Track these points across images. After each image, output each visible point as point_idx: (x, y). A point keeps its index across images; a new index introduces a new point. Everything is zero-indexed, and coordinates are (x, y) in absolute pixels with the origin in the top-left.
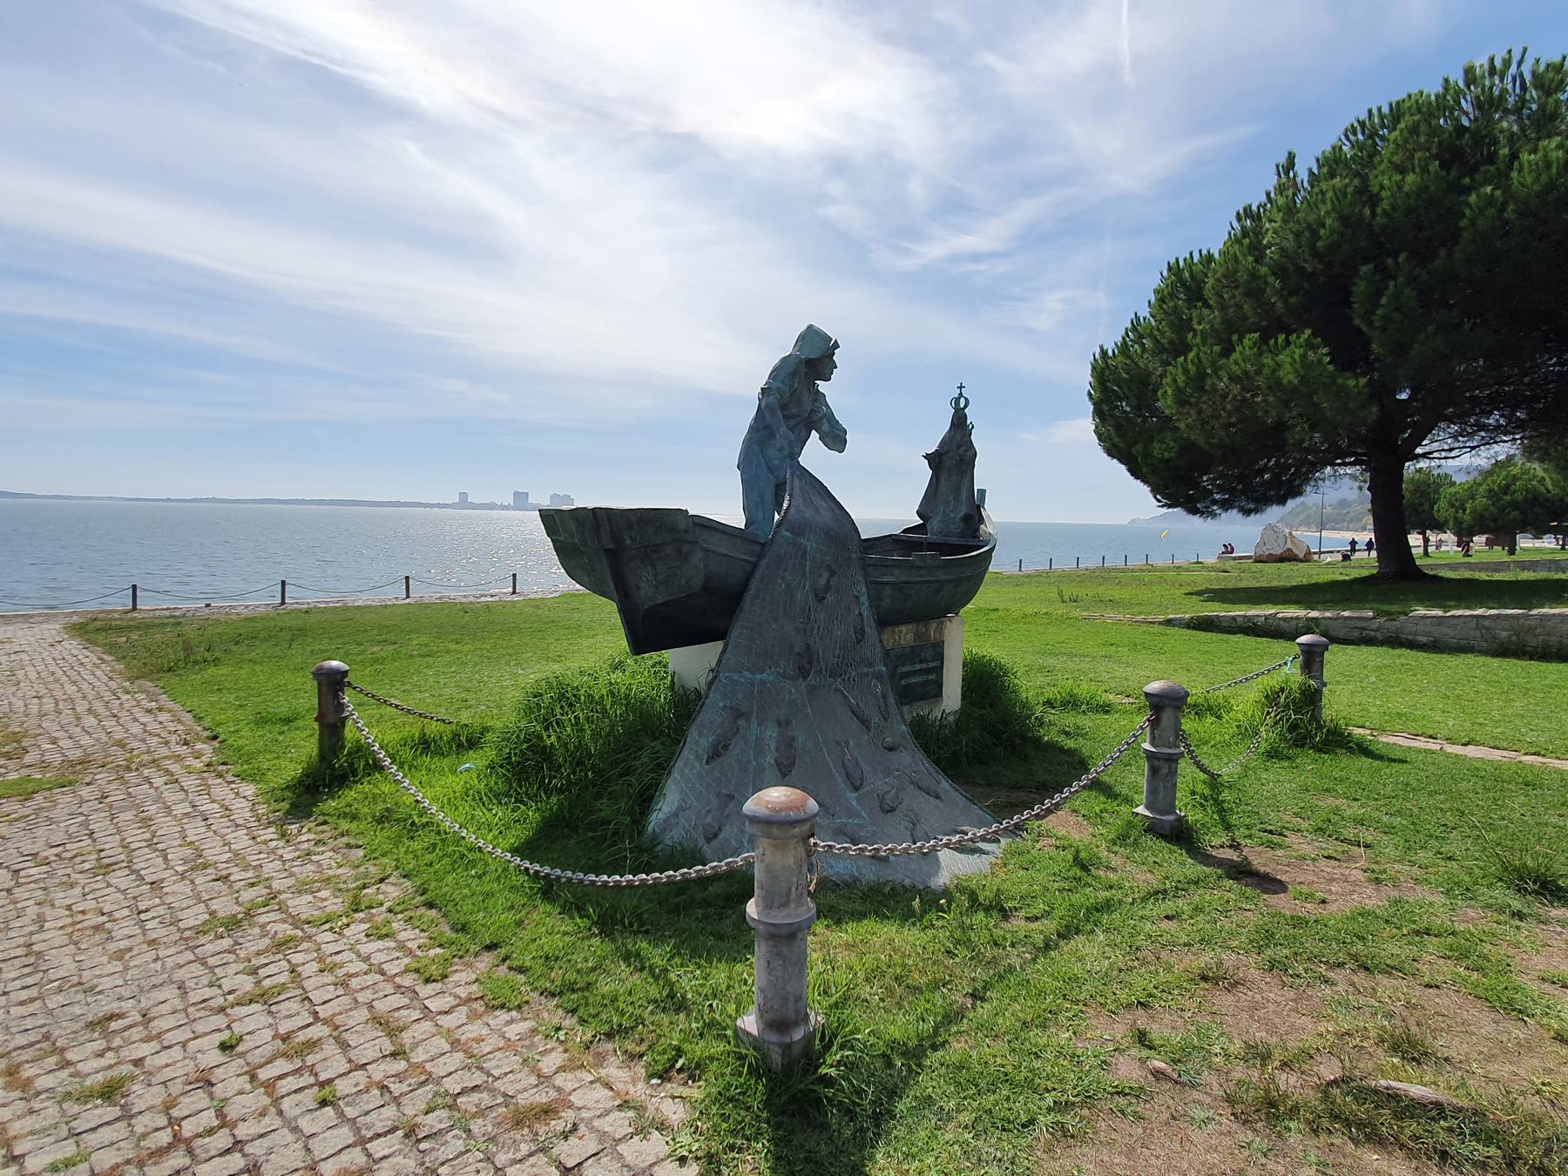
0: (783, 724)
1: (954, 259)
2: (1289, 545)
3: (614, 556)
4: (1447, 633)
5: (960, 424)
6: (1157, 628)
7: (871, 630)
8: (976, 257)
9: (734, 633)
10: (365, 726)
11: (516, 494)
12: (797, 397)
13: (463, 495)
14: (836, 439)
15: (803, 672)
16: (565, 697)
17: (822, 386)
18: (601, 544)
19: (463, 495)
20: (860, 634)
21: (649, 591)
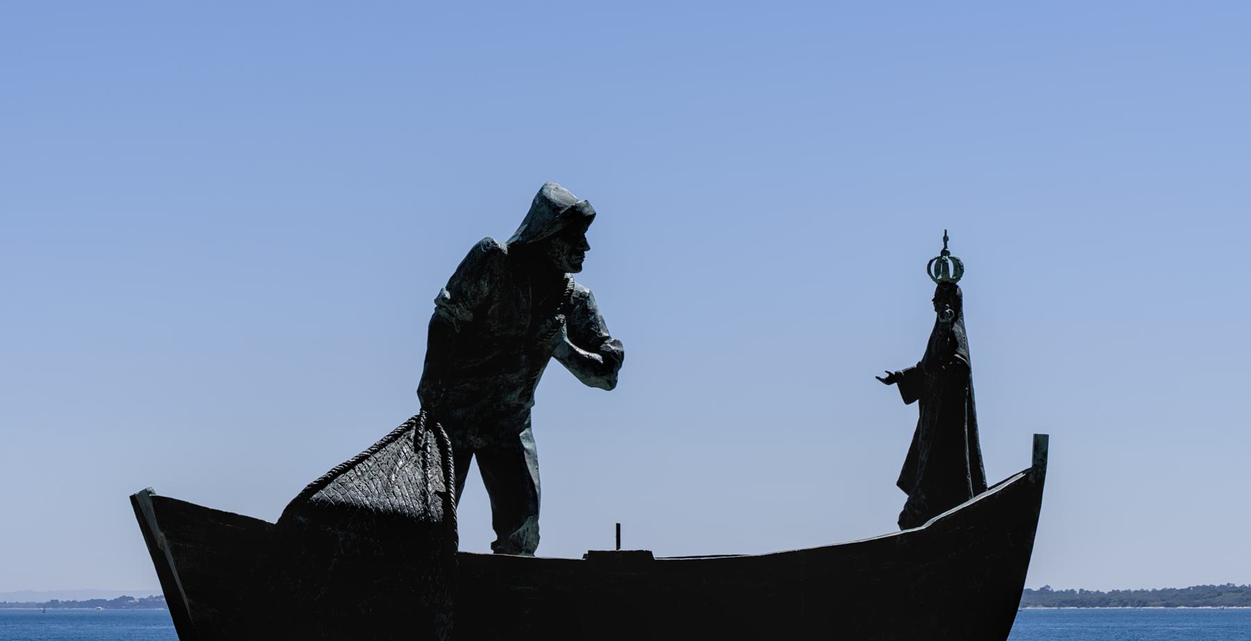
5: (948, 298)
17: (577, 282)
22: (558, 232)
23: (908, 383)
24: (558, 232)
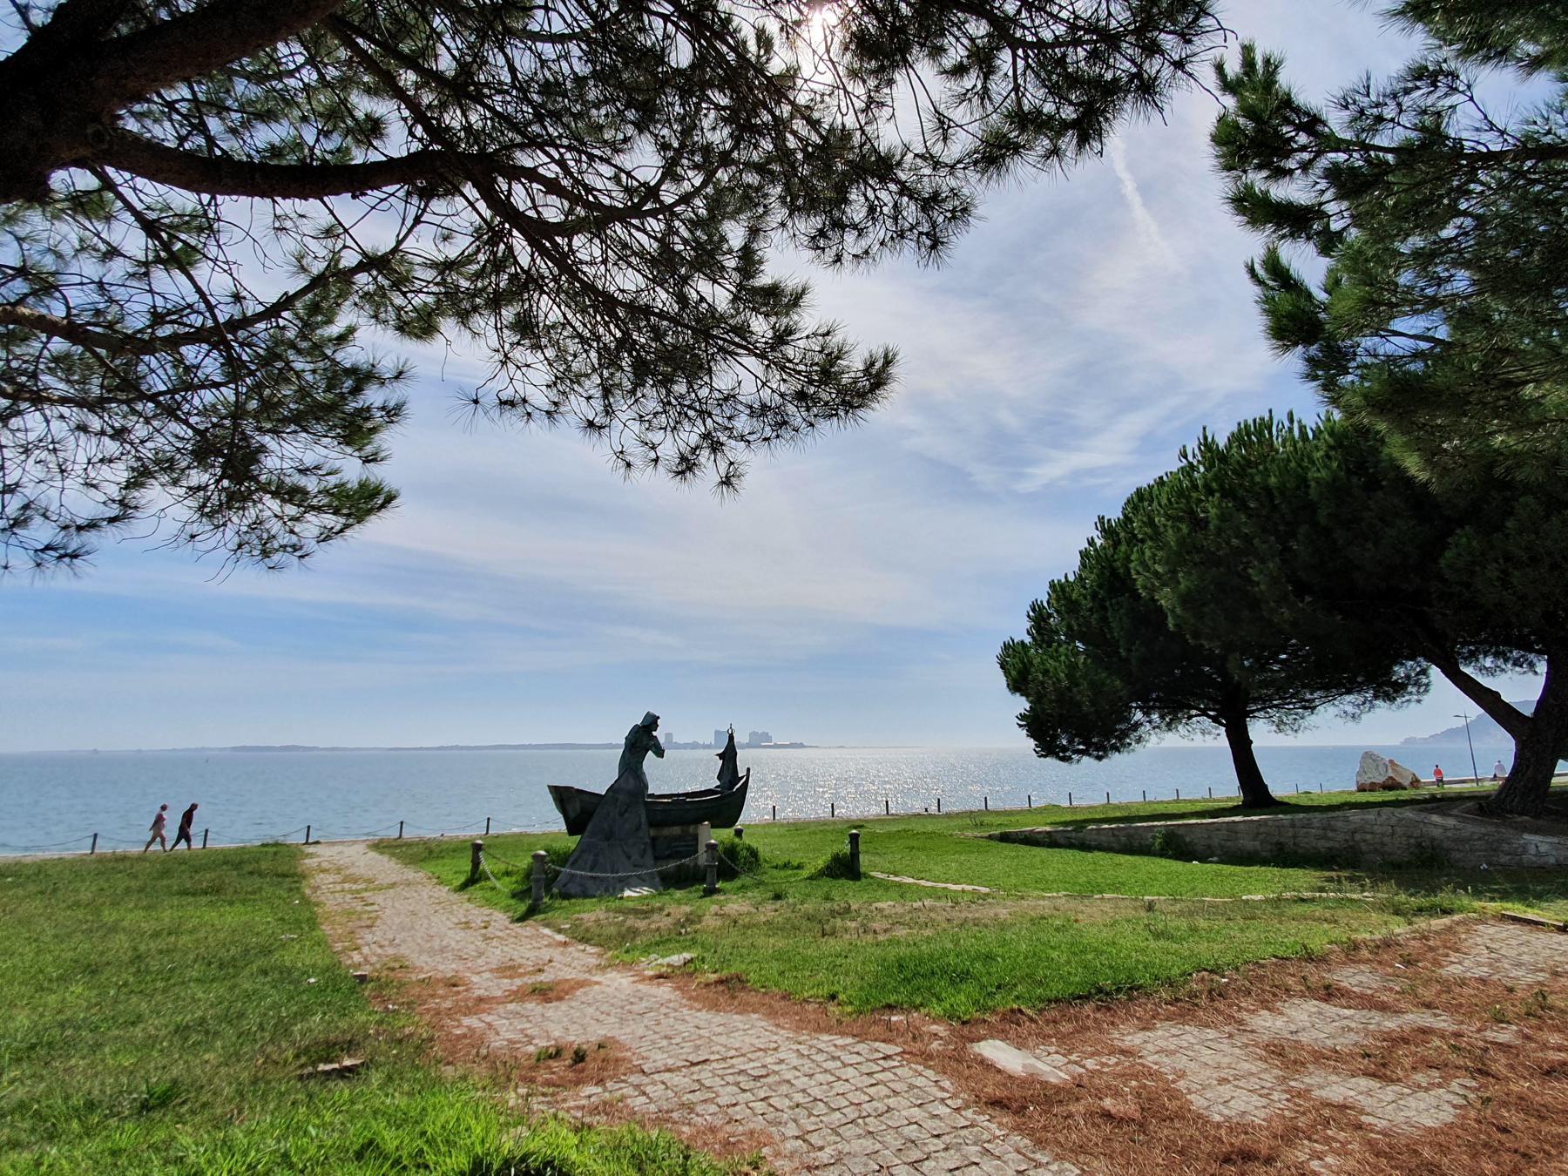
0: (596, 855)
1: (1076, 475)
2: (1390, 773)
7: (644, 827)
8: (1092, 472)
9: (589, 827)
10: (486, 865)
12: (643, 739)
14: (660, 753)
15: (608, 839)
18: (563, 796)
22: (651, 723)
23: (721, 756)
24: (651, 723)
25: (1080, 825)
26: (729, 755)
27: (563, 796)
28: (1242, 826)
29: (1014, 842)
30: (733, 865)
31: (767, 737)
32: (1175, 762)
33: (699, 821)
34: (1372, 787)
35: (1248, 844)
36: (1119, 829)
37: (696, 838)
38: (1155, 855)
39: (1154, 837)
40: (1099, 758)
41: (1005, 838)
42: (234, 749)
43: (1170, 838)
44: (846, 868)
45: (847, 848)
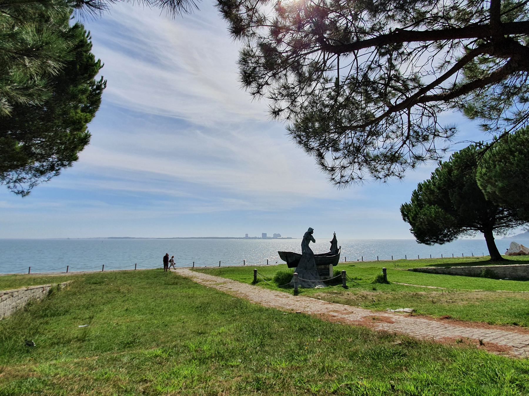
2: (521, 249)
3: (286, 257)
4: (458, 271)
5: (335, 236)
6: (406, 272)
7: (315, 265)
9: (299, 265)
10: (259, 277)
11: (263, 234)
12: (309, 237)
13: (247, 235)
14: (314, 241)
16: (281, 273)
18: (284, 255)
19: (247, 235)
20: (313, 266)
21: (290, 261)
25: (448, 265)
26: (334, 242)
27: (284, 255)
28: (520, 268)
29: (420, 272)
30: (340, 280)
31: (279, 235)
32: (469, 244)
33: (329, 264)
34: (515, 254)
35: (521, 273)
36: (465, 268)
37: (328, 269)
38: (482, 277)
39: (481, 271)
40: (441, 244)
41: (415, 270)
42: (109, 238)
43: (468, 269)
44: (383, 280)
45: (382, 273)
